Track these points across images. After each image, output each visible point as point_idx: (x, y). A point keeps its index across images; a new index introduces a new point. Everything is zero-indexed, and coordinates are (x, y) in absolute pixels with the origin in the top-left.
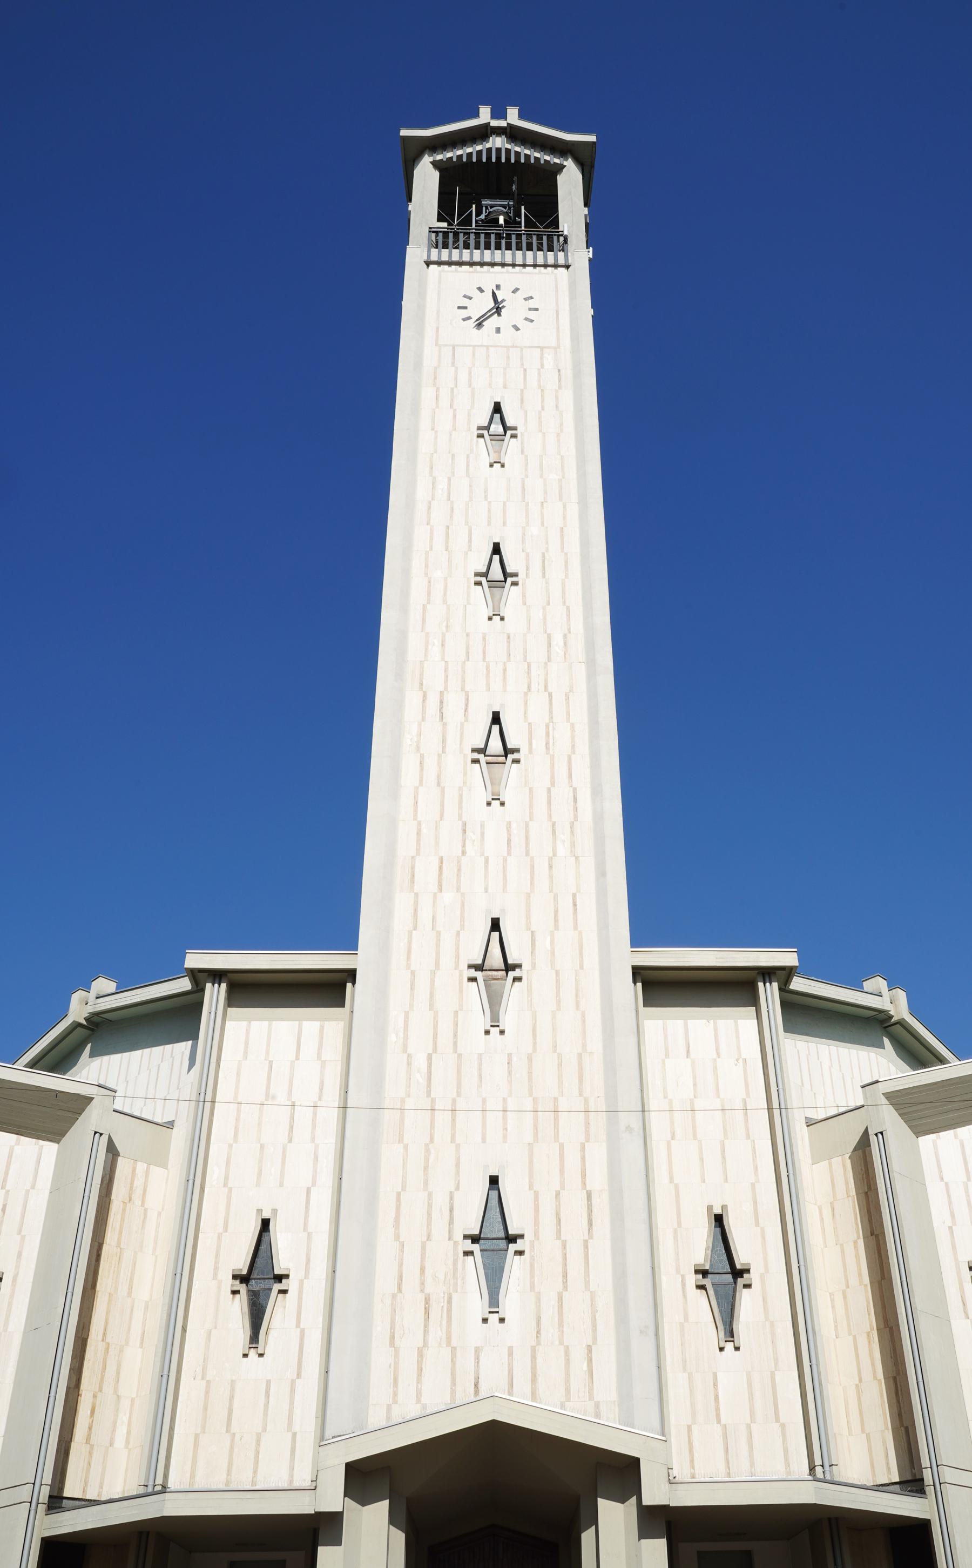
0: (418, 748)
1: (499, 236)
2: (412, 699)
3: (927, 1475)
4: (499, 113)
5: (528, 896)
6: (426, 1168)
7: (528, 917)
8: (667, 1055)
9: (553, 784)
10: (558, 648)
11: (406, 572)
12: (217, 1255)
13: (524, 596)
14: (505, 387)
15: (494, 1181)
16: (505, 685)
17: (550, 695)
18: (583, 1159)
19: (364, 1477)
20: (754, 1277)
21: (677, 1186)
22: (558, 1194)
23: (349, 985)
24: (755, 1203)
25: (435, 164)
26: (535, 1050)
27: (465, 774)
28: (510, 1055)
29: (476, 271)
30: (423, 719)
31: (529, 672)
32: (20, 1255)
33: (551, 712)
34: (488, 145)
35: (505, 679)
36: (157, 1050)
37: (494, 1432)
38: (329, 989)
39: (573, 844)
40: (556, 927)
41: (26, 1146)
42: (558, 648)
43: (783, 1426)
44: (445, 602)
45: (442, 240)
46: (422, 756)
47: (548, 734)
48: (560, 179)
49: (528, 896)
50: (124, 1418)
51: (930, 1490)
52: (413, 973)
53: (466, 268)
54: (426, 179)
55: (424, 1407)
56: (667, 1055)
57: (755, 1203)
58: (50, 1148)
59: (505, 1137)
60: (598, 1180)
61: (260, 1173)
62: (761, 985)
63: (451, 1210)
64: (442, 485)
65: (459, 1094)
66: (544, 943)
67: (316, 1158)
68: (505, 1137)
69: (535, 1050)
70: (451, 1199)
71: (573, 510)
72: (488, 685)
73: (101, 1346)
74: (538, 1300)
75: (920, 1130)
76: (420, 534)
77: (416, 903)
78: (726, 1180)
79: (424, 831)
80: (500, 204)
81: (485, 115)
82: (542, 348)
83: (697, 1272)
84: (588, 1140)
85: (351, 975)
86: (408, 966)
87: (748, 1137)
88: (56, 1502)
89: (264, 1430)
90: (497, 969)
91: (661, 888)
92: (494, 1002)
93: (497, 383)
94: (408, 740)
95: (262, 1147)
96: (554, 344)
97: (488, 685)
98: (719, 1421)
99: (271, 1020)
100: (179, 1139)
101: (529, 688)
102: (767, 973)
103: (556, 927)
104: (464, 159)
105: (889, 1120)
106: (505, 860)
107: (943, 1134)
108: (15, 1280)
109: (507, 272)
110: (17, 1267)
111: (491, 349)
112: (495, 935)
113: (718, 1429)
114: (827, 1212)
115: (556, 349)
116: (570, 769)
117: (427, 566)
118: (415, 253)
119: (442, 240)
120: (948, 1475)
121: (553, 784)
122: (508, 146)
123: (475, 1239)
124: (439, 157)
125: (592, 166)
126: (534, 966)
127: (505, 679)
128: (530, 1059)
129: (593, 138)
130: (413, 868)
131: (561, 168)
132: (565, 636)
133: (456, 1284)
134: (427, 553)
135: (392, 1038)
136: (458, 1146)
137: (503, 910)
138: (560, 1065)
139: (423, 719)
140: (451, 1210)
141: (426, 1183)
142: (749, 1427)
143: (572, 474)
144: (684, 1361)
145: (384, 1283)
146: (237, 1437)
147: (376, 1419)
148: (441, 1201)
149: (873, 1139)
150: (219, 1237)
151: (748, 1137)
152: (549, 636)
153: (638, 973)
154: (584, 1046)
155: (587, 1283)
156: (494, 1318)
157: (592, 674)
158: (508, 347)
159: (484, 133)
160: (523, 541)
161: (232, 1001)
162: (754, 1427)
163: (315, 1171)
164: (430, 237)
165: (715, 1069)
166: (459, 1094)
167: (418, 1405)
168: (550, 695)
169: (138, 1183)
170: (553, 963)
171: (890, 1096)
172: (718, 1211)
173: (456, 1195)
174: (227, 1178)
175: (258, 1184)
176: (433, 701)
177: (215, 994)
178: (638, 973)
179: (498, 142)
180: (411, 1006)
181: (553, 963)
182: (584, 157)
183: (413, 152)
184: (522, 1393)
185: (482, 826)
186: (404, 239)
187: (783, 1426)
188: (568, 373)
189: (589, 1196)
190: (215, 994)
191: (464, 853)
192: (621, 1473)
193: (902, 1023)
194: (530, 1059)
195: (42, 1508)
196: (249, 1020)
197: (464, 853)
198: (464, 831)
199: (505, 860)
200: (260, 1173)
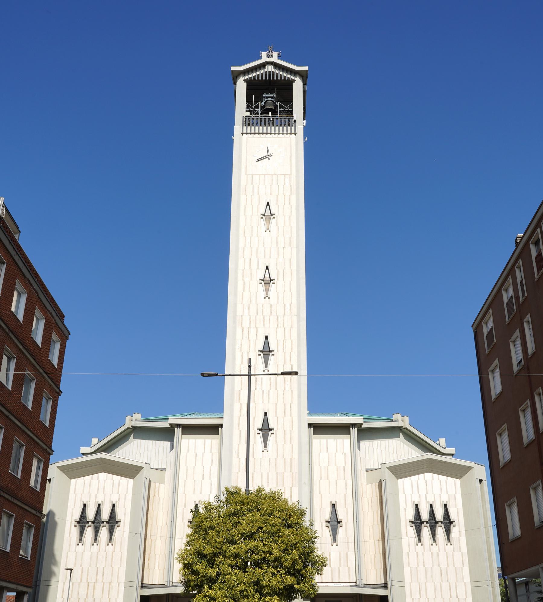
0: (241, 350)
1: (269, 120)
2: (239, 330)
3: (389, 583)
5: (276, 404)
8: (320, 452)
9: (285, 363)
10: (288, 310)
11: (236, 279)
12: (183, 515)
13: (277, 288)
14: (271, 194)
15: (267, 337)
17: (285, 329)
18: (291, 492)
20: (343, 524)
21: (321, 495)
23: (220, 429)
24: (345, 500)
25: (245, 81)
26: (277, 457)
27: (256, 359)
28: (270, 459)
29: (260, 137)
30: (243, 339)
31: (278, 320)
32: (125, 514)
33: (285, 336)
34: (266, 70)
35: (270, 322)
36: (158, 442)
38: (214, 429)
39: (291, 386)
41: (124, 480)
42: (288, 310)
43: (349, 568)
44: (249, 291)
46: (242, 353)
47: (283, 344)
48: (294, 85)
49: (276, 404)
50: (157, 561)
51: (389, 587)
52: (240, 431)
53: (257, 135)
54: (241, 87)
56: (320, 452)
57: (345, 500)
58: (131, 481)
61: (194, 489)
62: (351, 429)
64: (248, 240)
67: (211, 484)
69: (277, 457)
71: (295, 250)
72: (264, 325)
73: (150, 540)
75: (398, 478)
76: (241, 262)
77: (241, 407)
80: (270, 100)
81: (264, 58)
82: (285, 175)
85: (221, 426)
86: (239, 429)
87: (344, 479)
88: (143, 586)
90: (268, 216)
91: (319, 396)
92: (267, 291)
93: (268, 170)
94: (238, 347)
95: (195, 481)
96: (289, 173)
97: (264, 325)
99: (196, 439)
100: (168, 475)
102: (353, 425)
105: (388, 476)
106: (269, 392)
107: (406, 479)
109: (272, 137)
110: (125, 518)
111: (266, 176)
112: (268, 207)
114: (370, 501)
116: (291, 358)
117: (243, 276)
118: (238, 128)
120: (394, 583)
121: (285, 363)
122: (274, 70)
124: (246, 77)
125: (307, 77)
126: (277, 429)
127: (270, 322)
128: (276, 460)
129: (306, 69)
130: (240, 394)
132: (290, 305)
134: (243, 270)
135: (234, 453)
137: (268, 410)
138: (285, 462)
139: (243, 339)
142: (339, 568)
143: (294, 235)
149: (382, 481)
150: (183, 509)
151: (344, 479)
152: (285, 305)
153: (310, 425)
154: (292, 456)
156: (265, 451)
157: (299, 321)
159: (263, 65)
161: (183, 433)
163: (211, 488)
164: (243, 120)
165: (335, 456)
168: (285, 329)
169: (157, 490)
170: (283, 428)
172: (333, 503)
174: (184, 491)
175: (194, 493)
177: (178, 431)
178: (310, 425)
179: (269, 68)
180: (240, 442)
181: (283, 428)
182: (303, 75)
183: (236, 75)
187: (349, 568)
188: (294, 187)
190: (178, 431)
191: (256, 389)
193: (406, 428)
194: (276, 460)
195: (140, 588)
196: (189, 439)
197: (256, 389)
198: (256, 381)
199: (269, 392)
200: (194, 489)
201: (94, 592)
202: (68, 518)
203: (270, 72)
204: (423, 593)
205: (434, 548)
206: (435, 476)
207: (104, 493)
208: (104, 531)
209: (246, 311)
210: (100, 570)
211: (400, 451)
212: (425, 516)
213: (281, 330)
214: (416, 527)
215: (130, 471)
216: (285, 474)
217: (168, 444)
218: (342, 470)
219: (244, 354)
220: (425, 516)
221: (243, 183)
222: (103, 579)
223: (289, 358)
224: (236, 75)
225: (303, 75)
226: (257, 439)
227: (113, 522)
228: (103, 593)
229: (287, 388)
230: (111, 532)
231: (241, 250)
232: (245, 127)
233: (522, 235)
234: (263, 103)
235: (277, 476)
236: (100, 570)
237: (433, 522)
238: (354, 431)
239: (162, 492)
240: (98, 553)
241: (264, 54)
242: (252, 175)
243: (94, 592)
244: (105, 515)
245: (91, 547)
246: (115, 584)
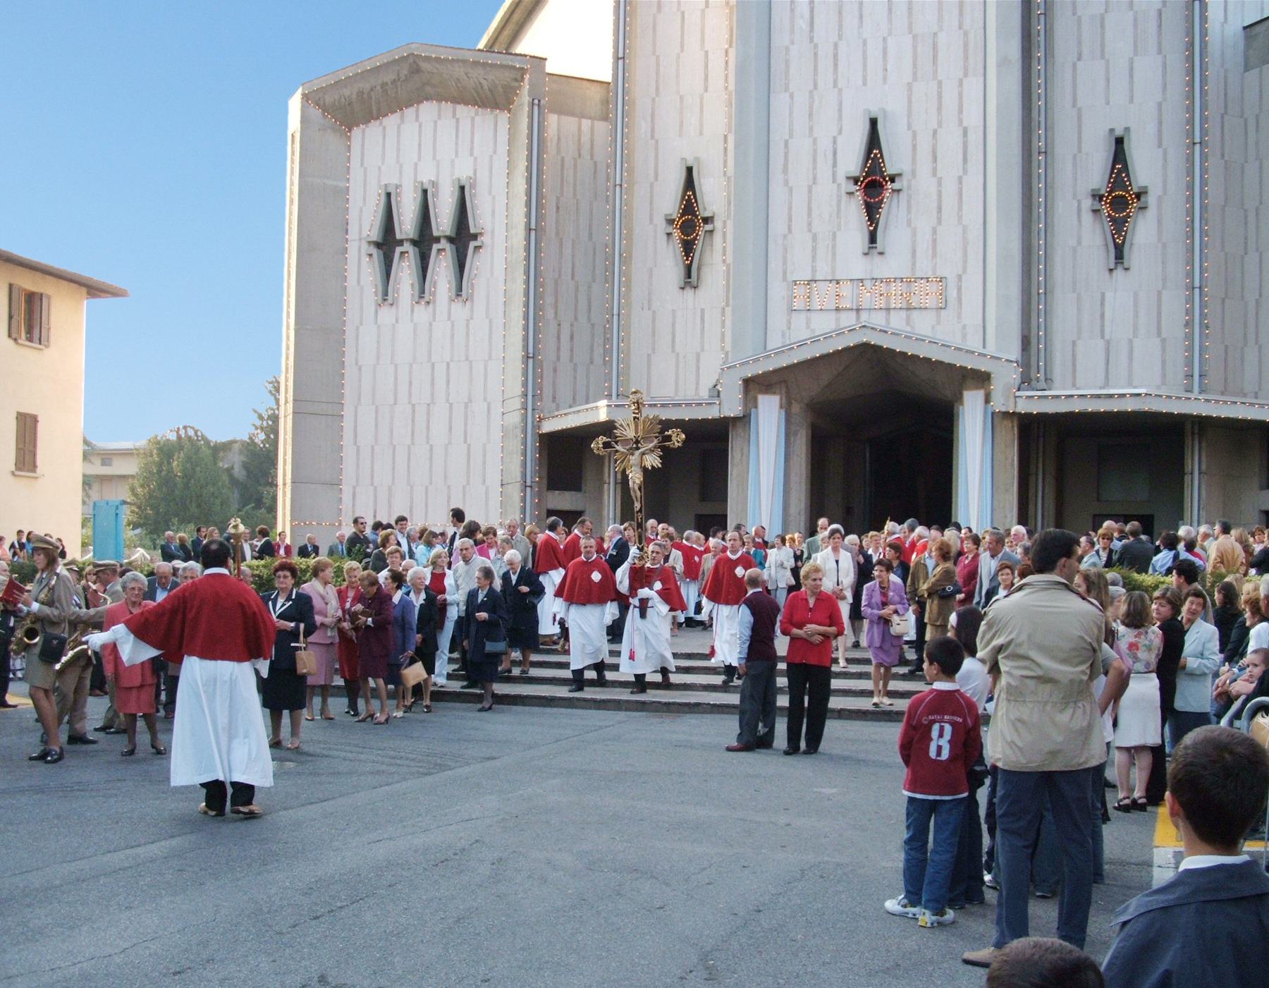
6: (811, 115)
7: (365, 176)
19: (754, 385)
20: (1151, 199)
21: (1080, 110)
22: (935, 132)
55: (813, 331)
59: (885, 79)
60: (973, 118)
63: (835, 153)
65: (840, 37)
68: (885, 79)
70: (835, 143)
74: (914, 234)
78: (1131, 101)
83: (1094, 196)
84: (966, 75)
89: (703, 350)
98: (1103, 337)
113: (1101, 343)
123: (856, 180)
126: (914, 173)
133: (839, 224)
136: (840, 91)
140: (835, 153)
141: (811, 129)
142: (1131, 342)
144: (1074, 283)
145: (973, 182)
146: (681, 356)
147: (774, 342)
148: (825, 144)
155: (960, 218)
162: (1136, 342)
166: (840, 37)
167: (812, 327)
172: (1119, 133)
173: (840, 140)
174: (653, 131)
201: (428, 428)
202: (353, 234)
207: (434, 158)
210: (440, 370)
216: (942, 39)
226: (1078, 232)
227: (463, 237)
228: (450, 429)
235: (915, 48)
236: (440, 370)
240: (431, 325)
243: (428, 428)
244: (443, 222)
245: (412, 311)
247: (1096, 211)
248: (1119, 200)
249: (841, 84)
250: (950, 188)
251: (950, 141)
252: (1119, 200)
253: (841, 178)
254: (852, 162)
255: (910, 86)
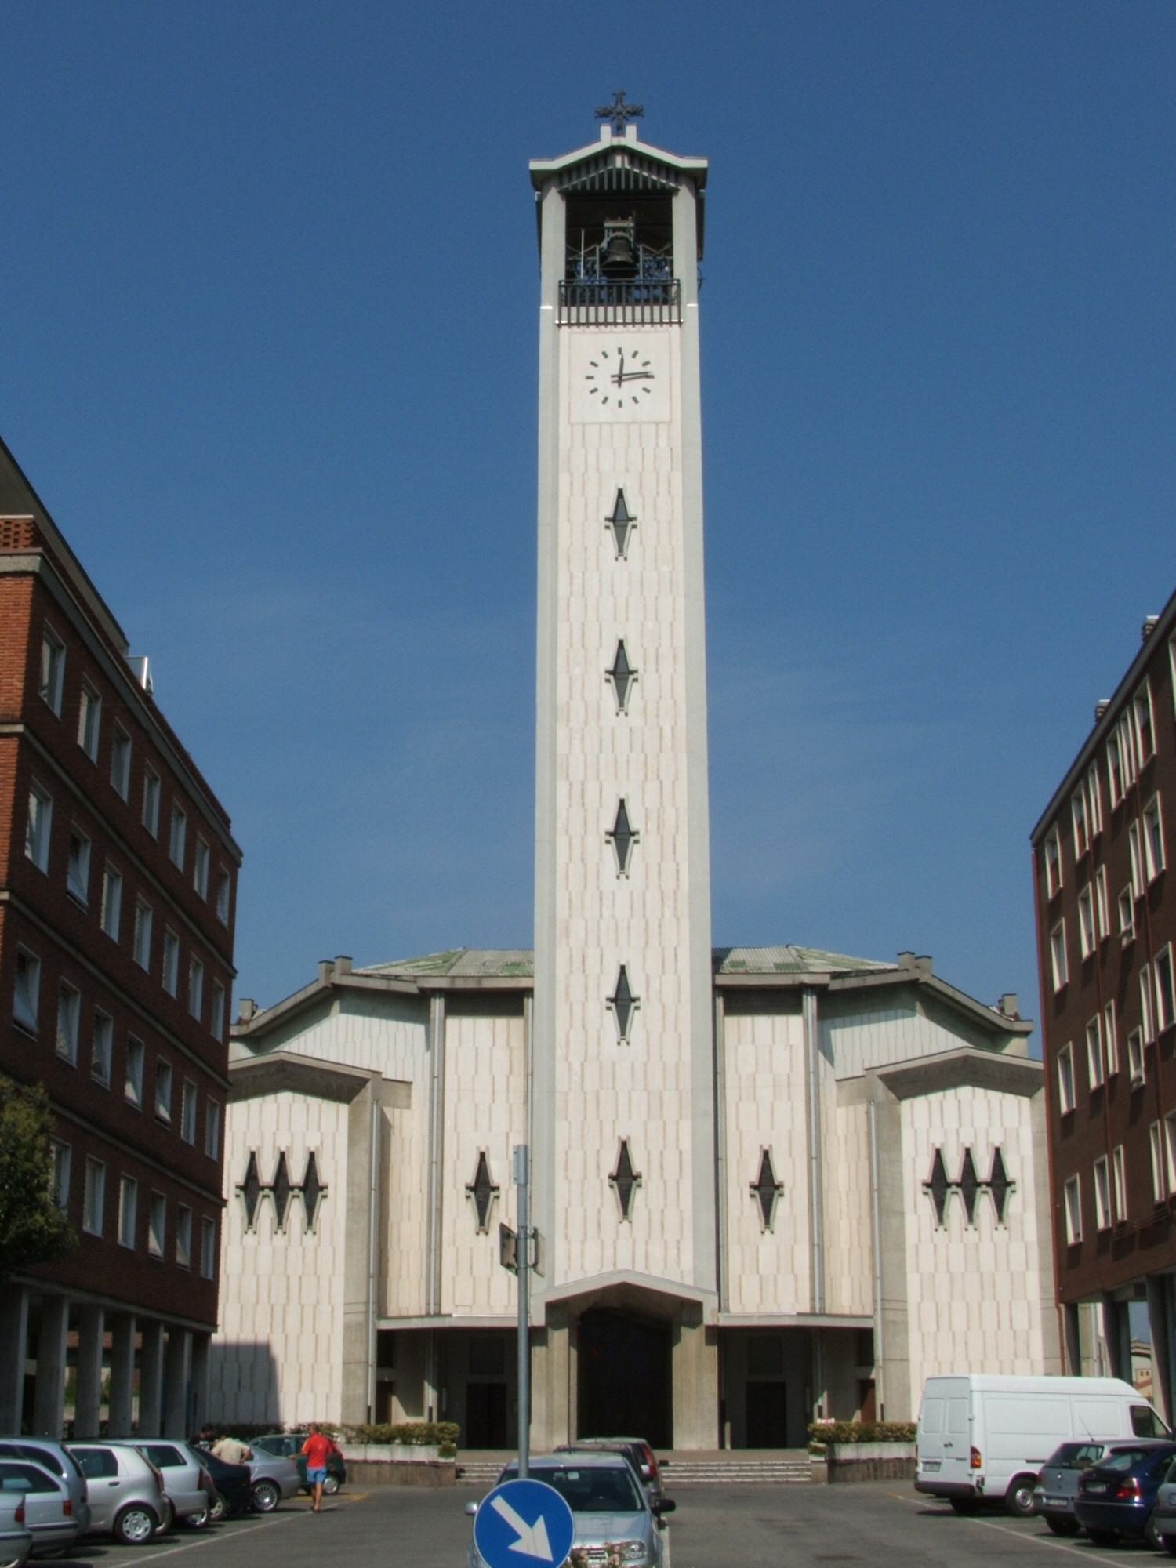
2: (562, 788)
4: (619, 131)
10: (667, 741)
16: (628, 775)
37: (625, 1290)
39: (675, 909)
40: (663, 972)
42: (667, 741)
45: (572, 295)
54: (554, 210)
64: (577, 581)
66: (655, 984)
75: (901, 1098)
79: (574, 898)
80: (619, 243)
81: (606, 138)
82: (657, 424)
93: (620, 409)
101: (646, 777)
103: (663, 972)
104: (588, 187)
108: (335, 1186)
113: (757, 1277)
115: (671, 422)
119: (572, 295)
126: (648, 999)
129: (702, 163)
131: (675, 191)
138: (664, 1069)
152: (661, 729)
158: (628, 424)
160: (642, 636)
161: (451, 1010)
165: (771, 1053)
171: (881, 1077)
176: (576, 790)
177: (437, 1005)
179: (620, 162)
184: (640, 1267)
185: (613, 894)
186: (536, 302)
189: (681, 1153)
192: (690, 1310)
203: (619, 171)
204: (944, 1322)
205: (971, 1234)
206: (980, 1091)
208: (296, 1208)
209: (577, 743)
210: (294, 1280)
211: (918, 1038)
212: (954, 1172)
213: (652, 787)
214: (995, 1194)
215: (336, 1085)
217: (419, 1029)
218: (785, 1082)
219: (574, 841)
220: (954, 1172)
221: (563, 445)
222: (300, 1298)
223: (671, 848)
224: (541, 181)
225: (696, 179)
226: (742, 1207)
229: (668, 913)
230: (310, 1209)
231: (562, 604)
232: (565, 309)
233: (1156, 617)
234: (604, 244)
236: (294, 1280)
237: (969, 1183)
238: (810, 1003)
239: (410, 1126)
241: (606, 131)
242: (584, 425)
246: (325, 1308)
247: (752, 1196)
248: (767, 1188)
249: (602, 777)
250: (671, 1186)
251: (671, 1158)
252: (767, 1188)
253: (602, 672)
254: (611, 1165)
255: (645, 1123)
